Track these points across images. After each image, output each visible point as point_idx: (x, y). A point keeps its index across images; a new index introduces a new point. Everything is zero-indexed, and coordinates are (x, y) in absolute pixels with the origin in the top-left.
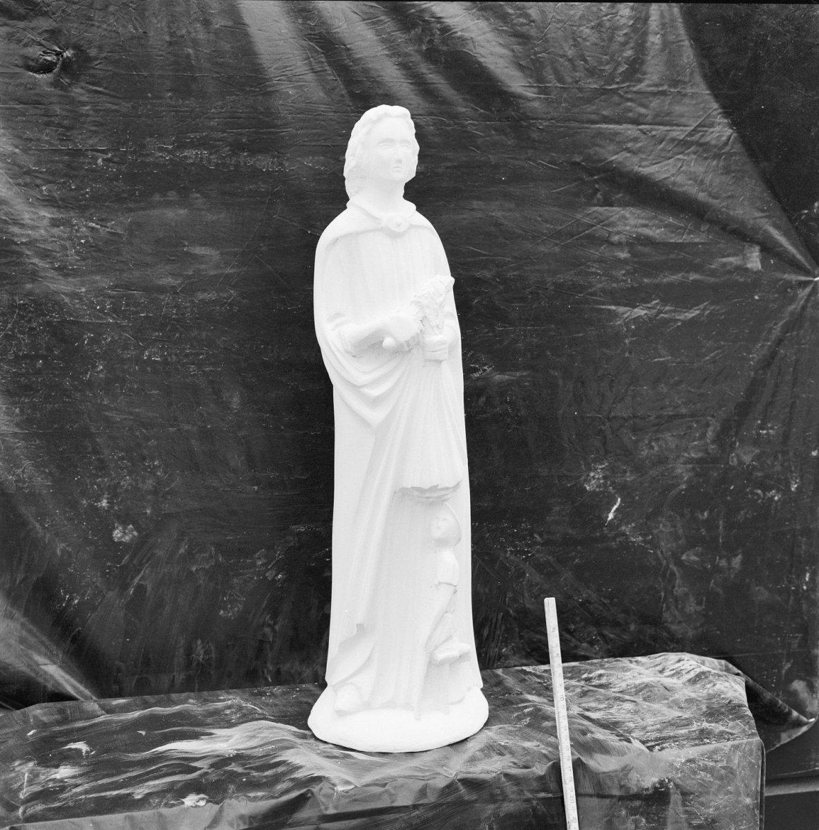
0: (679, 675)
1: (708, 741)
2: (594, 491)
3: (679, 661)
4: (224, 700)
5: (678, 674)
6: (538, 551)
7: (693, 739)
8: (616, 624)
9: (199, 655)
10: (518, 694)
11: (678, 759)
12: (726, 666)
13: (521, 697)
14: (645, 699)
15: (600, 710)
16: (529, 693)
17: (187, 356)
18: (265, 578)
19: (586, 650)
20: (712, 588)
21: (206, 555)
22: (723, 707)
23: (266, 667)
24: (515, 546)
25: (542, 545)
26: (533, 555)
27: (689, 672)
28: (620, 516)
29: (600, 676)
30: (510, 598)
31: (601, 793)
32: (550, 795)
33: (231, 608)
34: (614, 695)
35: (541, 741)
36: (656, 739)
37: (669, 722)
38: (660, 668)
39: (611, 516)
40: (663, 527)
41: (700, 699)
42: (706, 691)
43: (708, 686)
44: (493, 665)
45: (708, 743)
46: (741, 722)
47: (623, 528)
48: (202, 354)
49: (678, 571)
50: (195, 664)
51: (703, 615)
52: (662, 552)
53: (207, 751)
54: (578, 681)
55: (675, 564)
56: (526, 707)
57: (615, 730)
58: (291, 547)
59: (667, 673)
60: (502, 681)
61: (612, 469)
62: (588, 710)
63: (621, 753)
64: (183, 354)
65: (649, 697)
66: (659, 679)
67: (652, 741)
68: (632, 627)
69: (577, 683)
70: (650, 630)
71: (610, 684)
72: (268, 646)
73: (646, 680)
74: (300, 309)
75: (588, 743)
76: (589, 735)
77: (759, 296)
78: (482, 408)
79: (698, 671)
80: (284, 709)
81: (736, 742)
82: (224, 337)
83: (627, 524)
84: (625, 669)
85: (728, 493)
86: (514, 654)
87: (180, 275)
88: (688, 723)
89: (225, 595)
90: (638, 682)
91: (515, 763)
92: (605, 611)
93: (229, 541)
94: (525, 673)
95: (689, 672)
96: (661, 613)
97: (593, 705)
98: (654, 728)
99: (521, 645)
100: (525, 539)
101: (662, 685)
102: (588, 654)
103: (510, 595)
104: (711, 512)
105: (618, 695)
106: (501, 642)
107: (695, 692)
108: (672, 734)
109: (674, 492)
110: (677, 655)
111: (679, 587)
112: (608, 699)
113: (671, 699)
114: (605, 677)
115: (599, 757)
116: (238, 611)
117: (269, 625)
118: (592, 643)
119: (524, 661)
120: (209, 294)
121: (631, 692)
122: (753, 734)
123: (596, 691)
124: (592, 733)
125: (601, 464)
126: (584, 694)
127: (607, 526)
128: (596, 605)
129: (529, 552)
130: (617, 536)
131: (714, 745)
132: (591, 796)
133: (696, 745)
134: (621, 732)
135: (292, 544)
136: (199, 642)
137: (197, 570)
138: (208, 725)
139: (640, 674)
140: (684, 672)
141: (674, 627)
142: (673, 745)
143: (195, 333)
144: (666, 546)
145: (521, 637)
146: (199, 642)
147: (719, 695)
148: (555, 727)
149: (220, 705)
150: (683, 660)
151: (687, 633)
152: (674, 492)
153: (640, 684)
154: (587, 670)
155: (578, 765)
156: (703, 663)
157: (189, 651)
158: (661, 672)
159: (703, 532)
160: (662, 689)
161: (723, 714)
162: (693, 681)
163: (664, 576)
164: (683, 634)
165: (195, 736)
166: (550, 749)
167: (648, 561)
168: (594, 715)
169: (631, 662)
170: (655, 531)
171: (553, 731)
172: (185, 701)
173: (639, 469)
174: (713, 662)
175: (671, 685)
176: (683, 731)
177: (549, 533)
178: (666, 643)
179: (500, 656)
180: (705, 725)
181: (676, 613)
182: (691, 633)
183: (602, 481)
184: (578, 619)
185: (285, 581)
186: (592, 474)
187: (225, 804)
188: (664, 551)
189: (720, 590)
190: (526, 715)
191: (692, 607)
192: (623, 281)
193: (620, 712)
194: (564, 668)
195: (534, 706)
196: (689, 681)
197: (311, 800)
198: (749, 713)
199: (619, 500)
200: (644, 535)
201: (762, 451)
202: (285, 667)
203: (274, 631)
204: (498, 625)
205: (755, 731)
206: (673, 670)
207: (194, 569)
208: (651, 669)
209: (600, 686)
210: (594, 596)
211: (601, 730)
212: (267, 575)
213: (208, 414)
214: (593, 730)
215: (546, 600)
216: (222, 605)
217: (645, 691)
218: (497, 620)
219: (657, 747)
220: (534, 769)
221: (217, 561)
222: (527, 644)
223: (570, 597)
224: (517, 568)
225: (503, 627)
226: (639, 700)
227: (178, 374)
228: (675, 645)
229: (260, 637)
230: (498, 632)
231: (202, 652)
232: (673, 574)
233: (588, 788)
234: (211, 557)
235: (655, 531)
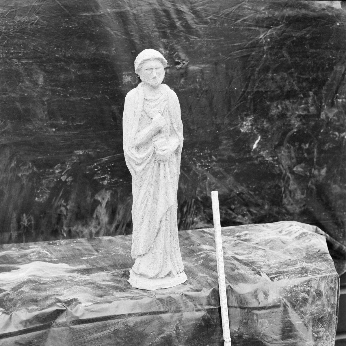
0: (290, 234)
1: (306, 275)
2: (246, 133)
3: (291, 226)
4: (32, 248)
5: (290, 233)
6: (214, 166)
7: (297, 274)
8: (257, 205)
9: (25, 222)
10: (198, 245)
11: (288, 286)
12: (316, 229)
13: (200, 247)
14: (270, 249)
15: (244, 254)
16: (204, 244)
17: (12, 54)
18: (61, 180)
19: (240, 219)
20: (310, 186)
21: (27, 167)
22: (315, 253)
23: (63, 229)
24: (202, 163)
25: (216, 162)
26: (212, 168)
27: (296, 232)
28: (260, 146)
29: (246, 234)
30: (199, 191)
31: (241, 306)
32: (212, 307)
33: (42, 196)
34: (253, 245)
35: (208, 274)
36: (276, 273)
37: (284, 262)
38: (279, 230)
39: (255, 146)
40: (283, 152)
41: (302, 249)
42: (305, 244)
43: (307, 241)
44: (189, 227)
45: (307, 276)
46: (326, 263)
47: (262, 153)
48: (20, 53)
49: (292, 177)
50: (22, 227)
51: (305, 201)
52: (283, 166)
53: (12, 279)
54: (233, 237)
55: (290, 173)
56: (201, 254)
57: (252, 267)
58: (75, 163)
59: (284, 233)
60: (190, 237)
61: (255, 121)
62: (237, 254)
63: (254, 282)
64: (9, 53)
65: (273, 247)
66: (278, 236)
67: (273, 274)
68: (266, 207)
69: (233, 239)
70: (276, 209)
71: (251, 239)
72: (63, 217)
73: (271, 237)
74: (77, 27)
75: (235, 276)
76: (236, 271)
77: (340, 24)
78: (183, 85)
79: (301, 232)
80: (65, 253)
81: (323, 275)
82: (33, 43)
83: (264, 150)
84: (260, 231)
85: (320, 134)
86: (201, 221)
87: (6, 7)
88: (295, 263)
89: (38, 189)
90: (267, 238)
91: (192, 289)
92: (251, 198)
93: (39, 159)
94: (204, 232)
95: (296, 232)
96: (282, 199)
97: (241, 251)
98: (275, 265)
99: (204, 216)
100: (207, 159)
101: (280, 240)
102: (241, 221)
103: (198, 189)
104: (310, 145)
105: (255, 246)
106: (194, 215)
107: (299, 244)
108: (285, 270)
109: (290, 134)
110: (290, 222)
111: (292, 185)
112: (249, 248)
113: (285, 248)
114: (249, 235)
115: (241, 284)
116: (46, 198)
117: (64, 206)
118: (244, 215)
119: (207, 225)
120: (23, 18)
121: (262, 244)
122: (333, 271)
123: (243, 243)
124: (238, 269)
125: (250, 117)
126: (236, 245)
127: (252, 152)
128: (246, 195)
129: (209, 166)
130: (258, 157)
131: (310, 277)
132: (235, 307)
133: (299, 277)
134: (255, 268)
135: (75, 161)
136: (24, 215)
137: (22, 176)
138: (18, 263)
139: (268, 233)
140: (293, 232)
141: (289, 207)
142: (285, 277)
143: (16, 41)
144: (285, 162)
145: (204, 212)
146: (24, 215)
147: (313, 247)
148: (216, 266)
149: (28, 251)
150: (293, 225)
151: (296, 210)
152: (290, 134)
153: (268, 240)
154: (238, 231)
155: (229, 290)
156: (304, 227)
157: (19, 220)
158: (280, 232)
159: (306, 155)
160: (281, 243)
161: (315, 258)
162: (298, 238)
163: (284, 179)
164: (293, 211)
165: (9, 270)
166: (213, 279)
167: (275, 171)
168: (240, 257)
169: (264, 226)
170: (279, 155)
171: (214, 269)
172: (9, 249)
173: (270, 120)
174: (309, 227)
175: (286, 240)
176: (292, 268)
177: (220, 155)
178: (285, 216)
179: (193, 223)
180: (305, 264)
181: (290, 199)
182: (298, 210)
183: (250, 127)
184: (236, 202)
185: (72, 181)
186: (244, 123)
187: (13, 314)
188: (284, 166)
189: (314, 187)
190: (200, 259)
191: (299, 195)
192: (263, 13)
193: (256, 256)
194: (222, 231)
195: (206, 253)
196: (296, 237)
197: (66, 311)
198: (330, 258)
199: (260, 137)
200: (273, 157)
201: (339, 112)
202: (74, 229)
203: (67, 209)
204: (192, 206)
205: (334, 269)
206: (287, 231)
207: (20, 175)
208: (275, 231)
209: (245, 240)
210: (246, 190)
211: (244, 267)
212: (62, 178)
213: (25, 87)
214: (239, 267)
215: (212, 192)
216: (37, 195)
217: (271, 244)
218: (191, 203)
219: (276, 278)
220: (202, 292)
221: (33, 170)
222: (208, 215)
223: (232, 191)
224: (203, 174)
225: (195, 207)
226: (267, 248)
227: (7, 65)
228: (290, 217)
229: (58, 212)
230: (192, 209)
231: (26, 221)
232: (289, 178)
233: (234, 303)
234: (29, 168)
235: (279, 155)
